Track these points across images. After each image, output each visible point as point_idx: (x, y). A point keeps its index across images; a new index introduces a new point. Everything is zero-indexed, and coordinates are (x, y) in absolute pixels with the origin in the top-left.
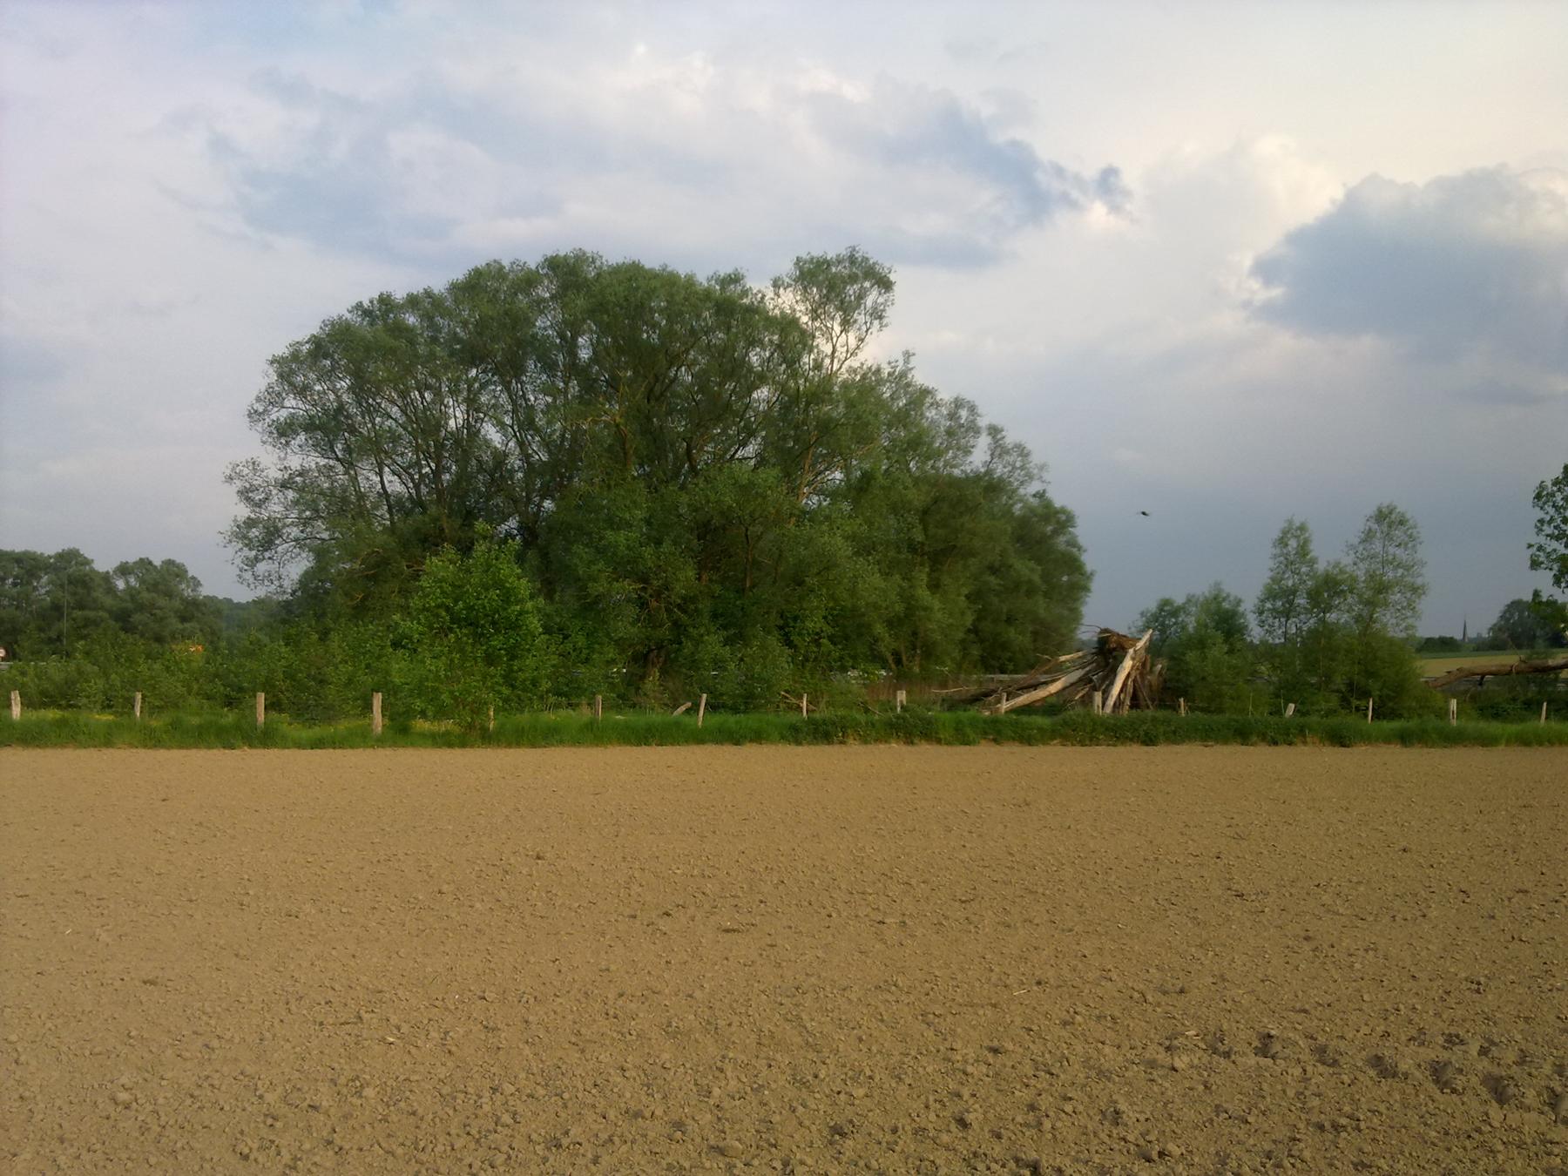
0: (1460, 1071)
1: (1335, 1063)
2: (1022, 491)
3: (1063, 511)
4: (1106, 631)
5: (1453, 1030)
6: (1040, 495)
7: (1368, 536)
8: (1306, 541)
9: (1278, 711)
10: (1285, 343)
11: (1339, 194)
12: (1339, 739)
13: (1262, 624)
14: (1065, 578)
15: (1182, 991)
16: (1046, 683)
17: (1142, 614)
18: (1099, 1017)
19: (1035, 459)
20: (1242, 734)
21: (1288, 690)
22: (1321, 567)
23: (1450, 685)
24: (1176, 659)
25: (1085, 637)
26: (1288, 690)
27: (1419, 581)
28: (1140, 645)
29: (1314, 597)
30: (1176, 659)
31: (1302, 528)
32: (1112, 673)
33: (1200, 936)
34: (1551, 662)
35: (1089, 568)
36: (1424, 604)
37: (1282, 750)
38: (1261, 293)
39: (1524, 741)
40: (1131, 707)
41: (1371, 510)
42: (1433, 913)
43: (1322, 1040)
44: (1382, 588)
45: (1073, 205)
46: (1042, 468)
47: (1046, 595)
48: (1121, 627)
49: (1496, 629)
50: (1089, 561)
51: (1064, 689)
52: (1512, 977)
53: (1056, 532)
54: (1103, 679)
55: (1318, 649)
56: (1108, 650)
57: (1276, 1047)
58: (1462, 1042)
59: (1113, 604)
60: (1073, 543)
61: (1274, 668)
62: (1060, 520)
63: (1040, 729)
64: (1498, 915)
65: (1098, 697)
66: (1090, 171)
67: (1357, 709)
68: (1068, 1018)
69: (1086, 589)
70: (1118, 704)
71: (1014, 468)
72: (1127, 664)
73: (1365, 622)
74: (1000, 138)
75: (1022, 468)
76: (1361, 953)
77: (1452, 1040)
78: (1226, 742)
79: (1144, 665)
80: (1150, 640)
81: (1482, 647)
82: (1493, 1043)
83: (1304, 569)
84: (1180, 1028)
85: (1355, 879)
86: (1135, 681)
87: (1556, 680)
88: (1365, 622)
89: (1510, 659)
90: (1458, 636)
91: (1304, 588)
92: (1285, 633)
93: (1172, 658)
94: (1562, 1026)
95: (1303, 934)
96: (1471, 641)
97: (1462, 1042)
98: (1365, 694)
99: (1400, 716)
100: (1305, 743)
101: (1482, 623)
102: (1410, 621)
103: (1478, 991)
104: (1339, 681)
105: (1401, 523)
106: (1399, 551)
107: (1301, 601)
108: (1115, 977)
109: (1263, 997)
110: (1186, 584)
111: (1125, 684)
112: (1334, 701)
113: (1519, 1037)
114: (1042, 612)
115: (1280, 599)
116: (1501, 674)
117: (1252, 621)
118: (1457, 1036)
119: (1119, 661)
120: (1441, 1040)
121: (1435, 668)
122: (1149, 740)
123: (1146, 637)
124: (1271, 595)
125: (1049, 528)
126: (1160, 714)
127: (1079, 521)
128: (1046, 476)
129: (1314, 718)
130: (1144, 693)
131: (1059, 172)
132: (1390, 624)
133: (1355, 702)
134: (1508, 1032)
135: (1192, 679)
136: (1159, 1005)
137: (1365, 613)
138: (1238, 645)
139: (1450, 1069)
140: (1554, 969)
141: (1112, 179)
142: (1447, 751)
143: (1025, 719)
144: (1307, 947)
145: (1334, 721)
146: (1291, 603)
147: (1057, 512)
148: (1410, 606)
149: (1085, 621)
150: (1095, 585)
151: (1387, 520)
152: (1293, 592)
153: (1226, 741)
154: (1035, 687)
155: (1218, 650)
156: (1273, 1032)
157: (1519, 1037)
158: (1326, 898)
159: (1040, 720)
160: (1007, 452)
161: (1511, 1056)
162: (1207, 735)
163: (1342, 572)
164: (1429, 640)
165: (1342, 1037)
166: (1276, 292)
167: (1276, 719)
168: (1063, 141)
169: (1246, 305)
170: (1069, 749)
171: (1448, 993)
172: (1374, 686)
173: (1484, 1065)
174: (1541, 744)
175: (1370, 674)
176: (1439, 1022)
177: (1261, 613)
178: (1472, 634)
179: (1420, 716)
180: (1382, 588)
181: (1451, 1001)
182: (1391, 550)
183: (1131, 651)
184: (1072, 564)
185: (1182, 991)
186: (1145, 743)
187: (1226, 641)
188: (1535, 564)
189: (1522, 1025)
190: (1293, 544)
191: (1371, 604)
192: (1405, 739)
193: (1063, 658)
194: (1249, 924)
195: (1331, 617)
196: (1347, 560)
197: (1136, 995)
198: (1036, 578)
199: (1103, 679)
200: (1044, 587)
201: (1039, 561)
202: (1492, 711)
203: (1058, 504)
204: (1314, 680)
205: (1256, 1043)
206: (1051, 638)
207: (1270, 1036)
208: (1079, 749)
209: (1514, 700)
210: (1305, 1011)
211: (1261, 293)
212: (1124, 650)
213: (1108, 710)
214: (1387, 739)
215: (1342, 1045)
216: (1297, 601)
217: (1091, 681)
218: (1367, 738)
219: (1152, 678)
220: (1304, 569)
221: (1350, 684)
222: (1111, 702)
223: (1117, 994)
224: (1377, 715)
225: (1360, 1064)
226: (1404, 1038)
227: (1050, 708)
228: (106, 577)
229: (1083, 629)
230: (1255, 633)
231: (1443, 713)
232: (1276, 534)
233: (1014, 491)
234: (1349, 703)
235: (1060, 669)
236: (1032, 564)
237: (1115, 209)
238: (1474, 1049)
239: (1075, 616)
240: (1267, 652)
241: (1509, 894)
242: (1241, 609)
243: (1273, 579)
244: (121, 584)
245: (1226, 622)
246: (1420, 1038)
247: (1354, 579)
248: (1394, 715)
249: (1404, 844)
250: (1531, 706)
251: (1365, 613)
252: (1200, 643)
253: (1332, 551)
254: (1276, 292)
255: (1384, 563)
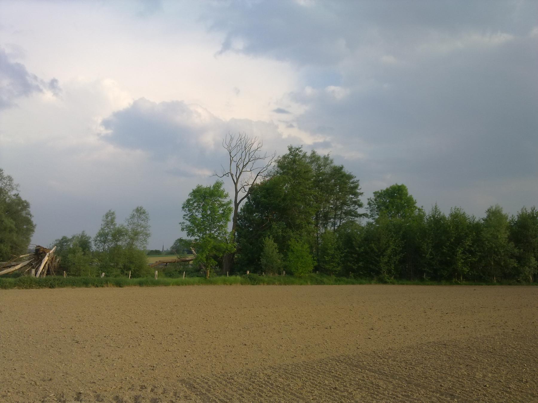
0: (144, 398)
1: (102, 400)
2: (9, 194)
3: (25, 202)
4: (39, 246)
5: (143, 384)
6: (17, 195)
7: (133, 216)
8: (114, 218)
9: (99, 275)
10: (111, 148)
11: (132, 102)
12: (119, 284)
13: (96, 245)
14: (25, 227)
15: (51, 380)
16: (14, 265)
17: (56, 241)
18: (17, 393)
19: (15, 182)
20: (86, 284)
21: (104, 268)
22: (117, 226)
23: (156, 266)
24: (65, 257)
25: (32, 248)
26: (104, 268)
27: (148, 232)
28: (51, 252)
29: (114, 236)
30: (65, 257)
31: (113, 213)
32: (41, 261)
33: (60, 358)
34: (187, 259)
35: (34, 223)
36: (149, 240)
37: (100, 289)
38: (103, 131)
39: (178, 284)
40: (46, 275)
41: (135, 208)
42: (142, 344)
43: (98, 393)
44: (136, 234)
45: (40, 91)
46: (18, 185)
47: (17, 232)
48: (45, 245)
49: (173, 248)
50: (34, 220)
51: (21, 268)
52: (164, 364)
53: (22, 210)
54: (37, 264)
55: (115, 252)
56: (39, 253)
57: (82, 397)
58: (146, 388)
59: (44, 236)
60: (29, 214)
61: (99, 260)
62: (25, 205)
63: (10, 283)
64: (163, 342)
65: (33, 271)
66: (47, 80)
67: (126, 274)
68: (5, 394)
69: (33, 231)
70: (42, 273)
71: (6, 185)
72: (46, 259)
73: (130, 245)
74: (12, 61)
75: (9, 185)
76: (117, 360)
77: (143, 387)
78: (80, 286)
79: (52, 259)
80: (56, 250)
81: (171, 253)
82: (155, 387)
83: (112, 227)
84: (48, 394)
85: (118, 334)
86: (48, 265)
87: (189, 264)
88: (130, 245)
89: (174, 258)
90: (161, 250)
91: (111, 233)
92: (103, 248)
93: (63, 256)
94: (178, 379)
95: (98, 354)
96: (165, 251)
97: (146, 388)
98: (129, 269)
99: (140, 276)
100: (108, 286)
101: (168, 245)
102: (145, 245)
103: (153, 370)
104: (121, 265)
105: (144, 213)
106: (142, 222)
107: (110, 238)
108: (26, 376)
109: (80, 379)
110: (71, 231)
111: (45, 266)
112: (119, 271)
113: (164, 384)
114: (15, 239)
115: (103, 236)
116: (173, 263)
117: (93, 243)
118: (144, 386)
119: (43, 257)
120: (139, 388)
121: (152, 260)
122: (52, 286)
123: (54, 249)
124: (100, 235)
125: (20, 208)
126: (57, 277)
127: (31, 206)
128: (19, 189)
129: (111, 278)
130: (52, 270)
131: (35, 78)
132: (139, 246)
133: (126, 272)
134: (161, 382)
135: (70, 264)
136: (41, 386)
137: (131, 242)
138: (87, 252)
139: (140, 398)
140: (178, 360)
141: (55, 83)
142: (154, 288)
143: (4, 279)
144: (98, 359)
145: (118, 279)
146: (106, 238)
147: (23, 202)
148: (145, 240)
149: (31, 243)
150: (36, 230)
151: (140, 212)
152: (107, 234)
153: (80, 286)
154: (10, 267)
155: (80, 254)
156: (81, 392)
157: (164, 384)
158: (108, 341)
159: (11, 280)
160: (4, 179)
161: (160, 391)
162: (73, 284)
163: (123, 228)
164: (152, 251)
165: (106, 391)
166: (110, 132)
167: (98, 278)
168: (36, 67)
169: (99, 135)
170: (21, 290)
171: (143, 371)
172: (132, 267)
173: (152, 395)
174: (183, 285)
175: (131, 262)
176: (139, 382)
177: (96, 241)
178: (165, 249)
179: (147, 276)
180: (136, 234)
181: (144, 374)
182: (140, 221)
183: (48, 254)
184: (28, 222)
185: (51, 380)
186: (50, 287)
187: (83, 251)
188: (183, 229)
189: (166, 380)
190: (110, 218)
191: (132, 239)
192: (141, 284)
193: (21, 256)
194: (79, 352)
195: (119, 243)
196: (125, 224)
197: (33, 383)
198: (13, 226)
199: (37, 264)
200: (16, 229)
201: (15, 219)
202: (169, 275)
203: (23, 199)
204: (112, 264)
205: (75, 396)
206: (17, 249)
207: (80, 393)
208: (25, 290)
209: (176, 271)
210: (94, 383)
211: (103, 131)
212: (45, 254)
213: (38, 276)
214: (135, 285)
215: (105, 394)
216: (108, 238)
217: (32, 264)
218: (128, 284)
219: (55, 264)
220: (112, 227)
221: (124, 266)
222: (39, 272)
223: (25, 383)
224: (133, 276)
225: (111, 399)
226: (127, 389)
227: (15, 275)
228: (416, 208)
229: (30, 245)
230: (94, 248)
231: (153, 276)
232: (105, 213)
233: (7, 193)
234: (124, 272)
235: (21, 260)
236: (12, 220)
237: (56, 94)
238: (149, 390)
239: (28, 241)
240: (97, 254)
241: (167, 335)
242: (90, 240)
243: (102, 229)
244: (377, 217)
245: (84, 244)
246: (132, 388)
247: (127, 230)
248: (139, 276)
249: (136, 320)
250: (181, 272)
251: (131, 242)
252: (74, 252)
253: (121, 222)
254: (110, 132)
255: (138, 225)
